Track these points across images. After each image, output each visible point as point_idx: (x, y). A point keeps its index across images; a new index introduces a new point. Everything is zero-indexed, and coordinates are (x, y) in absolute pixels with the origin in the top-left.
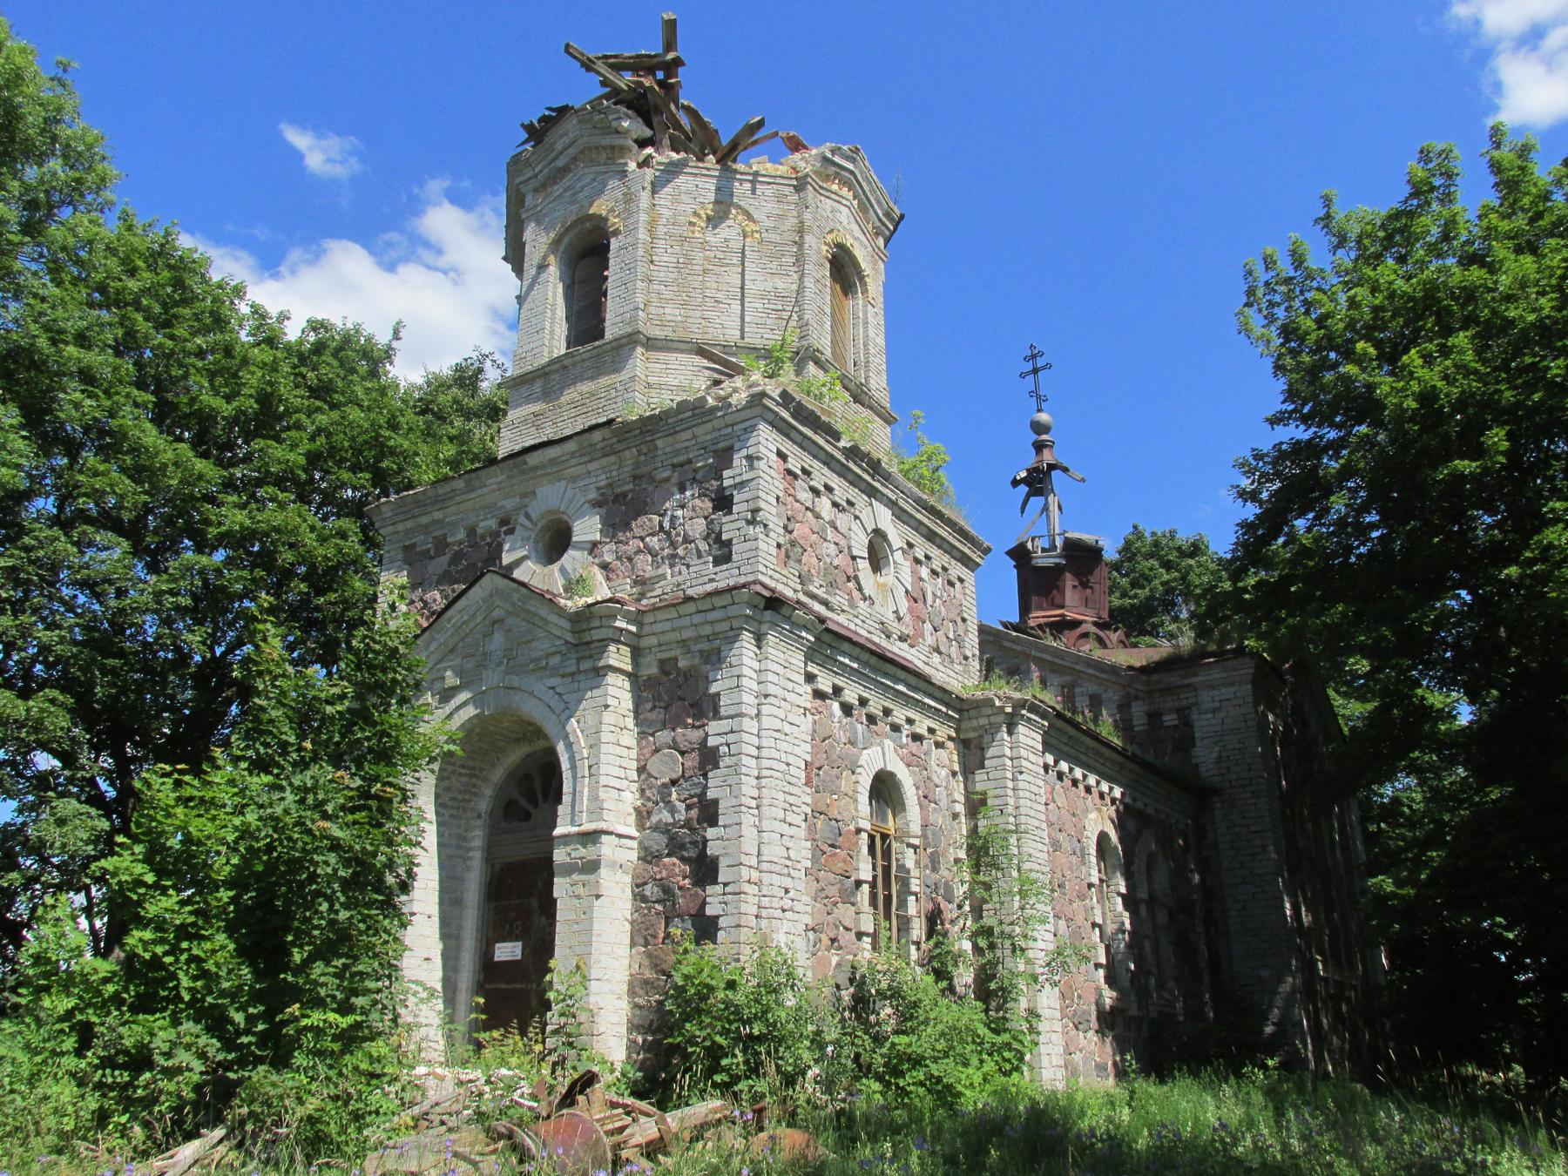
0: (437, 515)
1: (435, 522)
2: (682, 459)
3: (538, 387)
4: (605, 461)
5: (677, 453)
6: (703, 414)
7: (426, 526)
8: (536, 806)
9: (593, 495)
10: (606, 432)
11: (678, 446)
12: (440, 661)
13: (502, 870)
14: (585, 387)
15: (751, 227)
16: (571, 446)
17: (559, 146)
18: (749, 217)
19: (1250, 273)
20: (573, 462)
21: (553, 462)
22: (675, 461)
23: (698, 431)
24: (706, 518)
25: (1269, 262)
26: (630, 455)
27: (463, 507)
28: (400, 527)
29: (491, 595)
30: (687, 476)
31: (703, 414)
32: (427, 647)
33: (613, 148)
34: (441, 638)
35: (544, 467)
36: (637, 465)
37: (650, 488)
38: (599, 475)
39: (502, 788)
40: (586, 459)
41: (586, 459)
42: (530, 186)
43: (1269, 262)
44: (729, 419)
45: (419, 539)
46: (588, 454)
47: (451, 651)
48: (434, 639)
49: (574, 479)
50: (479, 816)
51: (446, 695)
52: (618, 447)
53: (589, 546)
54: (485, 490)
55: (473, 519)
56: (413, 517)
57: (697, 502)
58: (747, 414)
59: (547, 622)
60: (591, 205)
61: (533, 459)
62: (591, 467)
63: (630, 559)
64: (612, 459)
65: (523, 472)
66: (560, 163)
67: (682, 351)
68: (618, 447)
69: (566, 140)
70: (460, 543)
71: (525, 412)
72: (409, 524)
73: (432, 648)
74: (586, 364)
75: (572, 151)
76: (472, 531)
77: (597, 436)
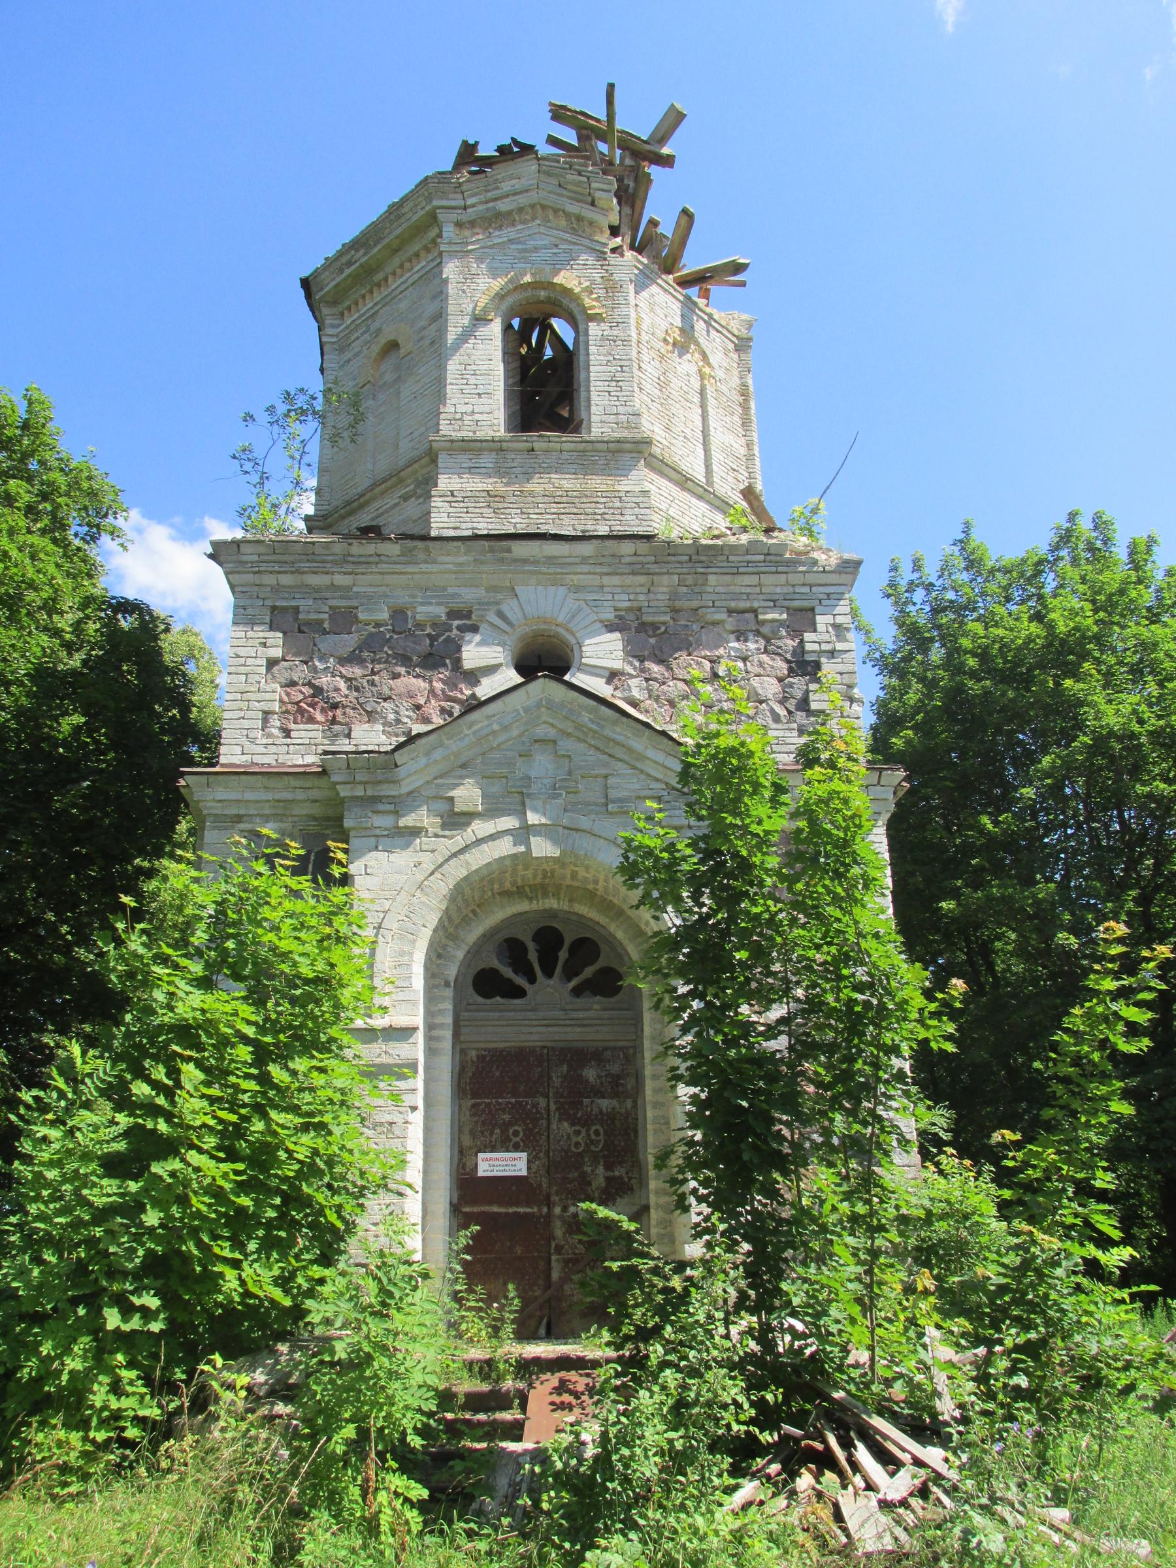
0: (340, 580)
1: (333, 587)
2: (743, 605)
3: (488, 460)
4: (629, 580)
5: (736, 596)
6: (777, 564)
7: (317, 589)
8: (532, 980)
9: (610, 615)
10: (642, 547)
11: (737, 589)
12: (441, 776)
13: (481, 1058)
14: (567, 482)
15: (707, 370)
16: (587, 549)
17: (506, 187)
18: (704, 356)
19: (895, 569)
20: (585, 568)
21: (551, 560)
22: (733, 604)
23: (767, 579)
24: (780, 680)
25: (917, 566)
26: (666, 583)
27: (389, 579)
28: (269, 580)
29: (539, 705)
30: (747, 624)
31: (777, 564)
32: (427, 754)
33: (579, 219)
34: (453, 745)
35: (536, 562)
36: (674, 596)
37: (695, 627)
38: (621, 592)
39: (475, 952)
40: (605, 570)
41: (605, 570)
42: (454, 216)
43: (917, 566)
44: (810, 578)
45: (304, 604)
46: (614, 566)
47: (463, 766)
48: (441, 745)
49: (577, 589)
50: (447, 984)
51: (455, 820)
52: (655, 568)
53: (607, 674)
54: (435, 568)
55: (402, 598)
56: (298, 572)
57: (764, 657)
58: (835, 578)
59: (641, 757)
60: (557, 272)
61: (521, 549)
62: (606, 580)
63: (672, 704)
64: (642, 579)
65: (502, 561)
66: (503, 206)
67: (670, 480)
68: (655, 568)
69: (517, 184)
70: (378, 625)
71: (481, 487)
72: (286, 580)
73: (438, 755)
74: (565, 456)
75: (522, 200)
76: (399, 614)
77: (627, 548)
